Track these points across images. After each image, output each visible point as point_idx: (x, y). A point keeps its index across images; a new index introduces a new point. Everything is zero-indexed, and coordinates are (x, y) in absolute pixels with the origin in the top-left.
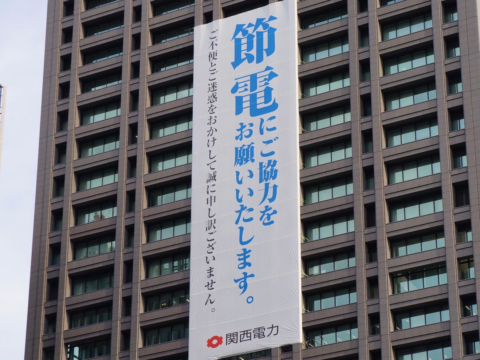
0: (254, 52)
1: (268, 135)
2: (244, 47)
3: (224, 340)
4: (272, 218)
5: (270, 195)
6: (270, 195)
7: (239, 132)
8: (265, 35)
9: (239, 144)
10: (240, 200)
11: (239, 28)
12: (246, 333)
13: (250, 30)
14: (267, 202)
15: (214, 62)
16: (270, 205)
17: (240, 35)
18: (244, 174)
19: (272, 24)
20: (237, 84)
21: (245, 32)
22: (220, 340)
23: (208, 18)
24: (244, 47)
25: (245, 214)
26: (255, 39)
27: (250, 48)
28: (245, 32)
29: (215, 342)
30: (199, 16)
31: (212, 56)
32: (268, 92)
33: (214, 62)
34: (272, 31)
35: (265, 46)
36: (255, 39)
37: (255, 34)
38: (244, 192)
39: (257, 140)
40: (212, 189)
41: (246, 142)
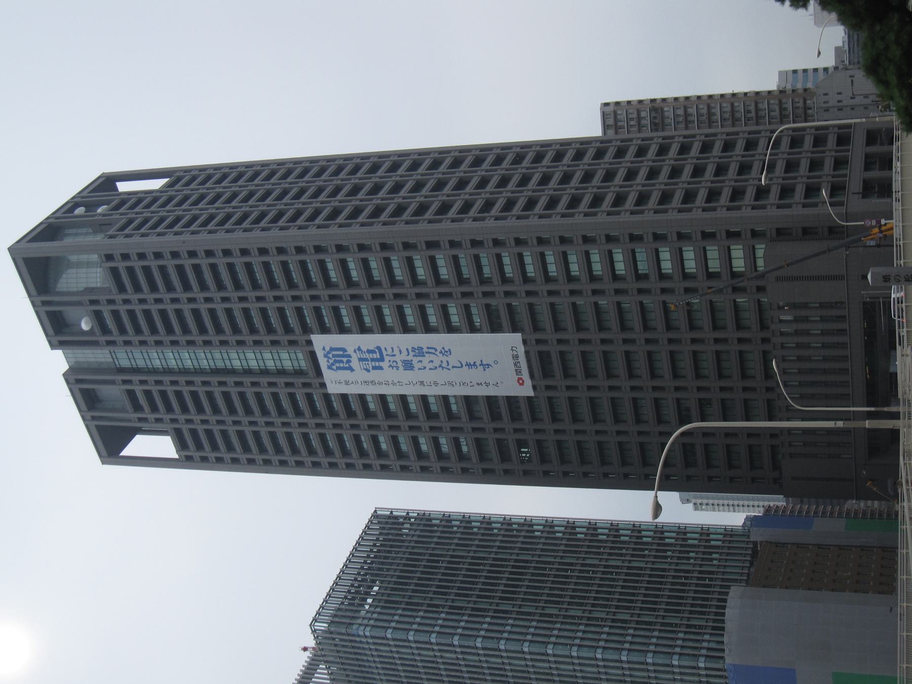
0: (345, 360)
1: (396, 352)
2: (341, 365)
3: (520, 376)
4: (447, 349)
5: (433, 351)
6: (433, 351)
7: (395, 368)
8: (334, 353)
9: (401, 368)
10: (436, 368)
11: (329, 367)
12: (515, 365)
13: (331, 361)
14: (438, 353)
15: (350, 382)
16: (439, 350)
17: (334, 367)
18: (420, 365)
19: (327, 349)
20: (364, 369)
21: (333, 364)
22: (519, 379)
23: (323, 385)
24: (341, 365)
25: (444, 365)
26: (337, 359)
27: (342, 362)
28: (333, 364)
29: (521, 382)
30: (322, 391)
31: (347, 383)
32: (369, 351)
33: (350, 382)
34: (332, 349)
35: (341, 353)
36: (337, 359)
37: (333, 359)
38: (431, 365)
39: (399, 358)
40: (429, 384)
41: (400, 364)
